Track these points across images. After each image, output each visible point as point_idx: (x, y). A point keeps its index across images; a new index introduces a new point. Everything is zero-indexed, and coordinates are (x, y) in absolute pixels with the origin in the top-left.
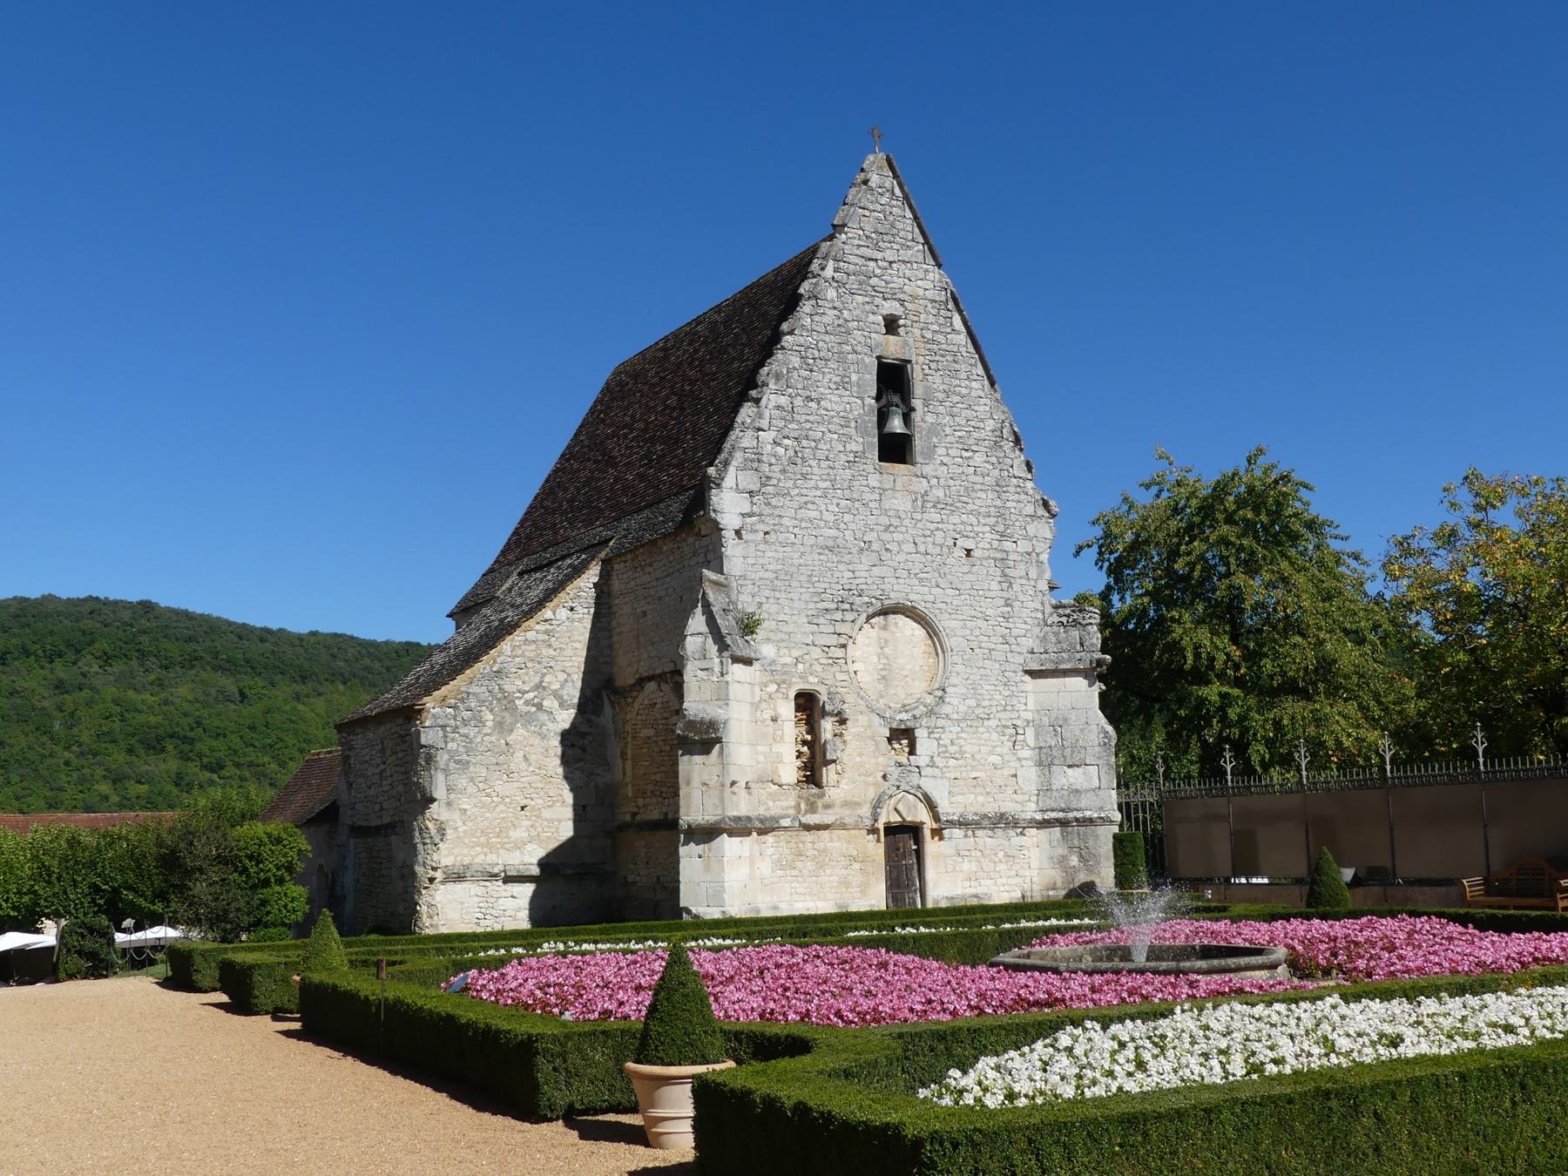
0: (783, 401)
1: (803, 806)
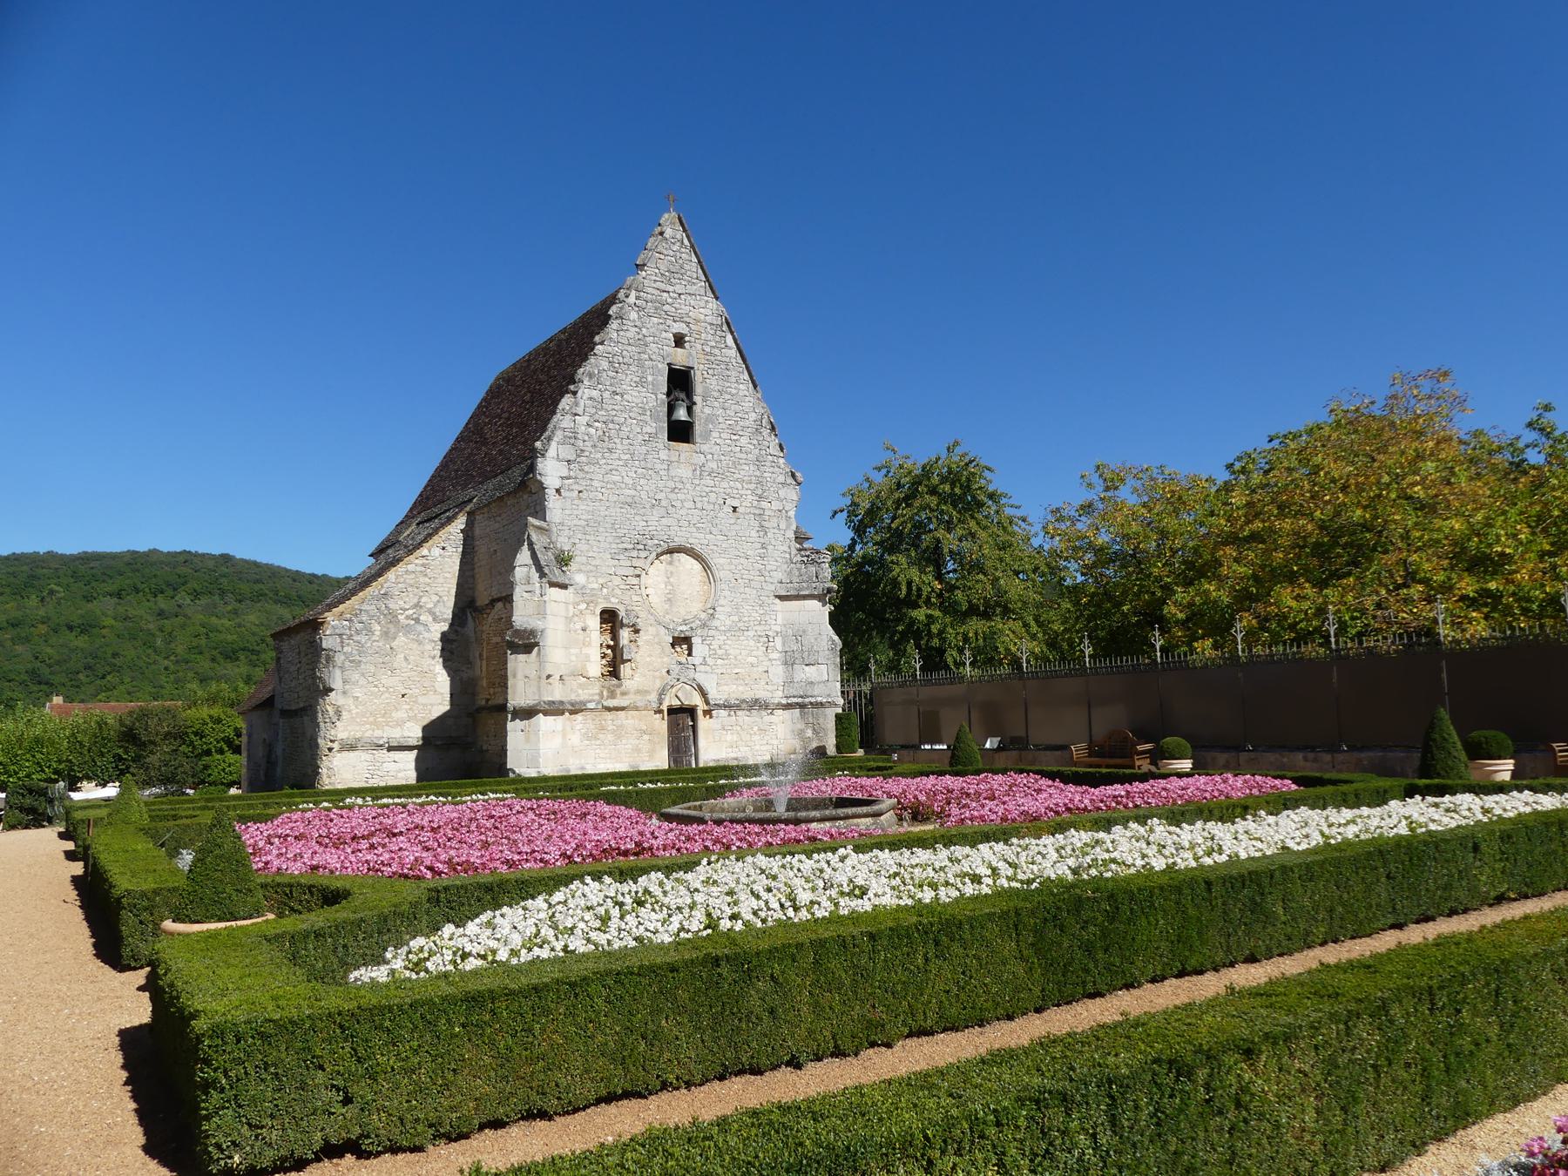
0: (595, 394)
1: (605, 693)
